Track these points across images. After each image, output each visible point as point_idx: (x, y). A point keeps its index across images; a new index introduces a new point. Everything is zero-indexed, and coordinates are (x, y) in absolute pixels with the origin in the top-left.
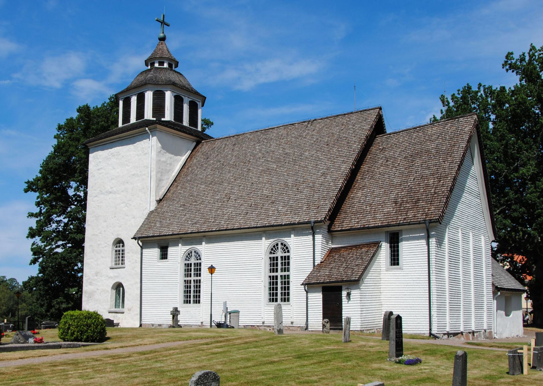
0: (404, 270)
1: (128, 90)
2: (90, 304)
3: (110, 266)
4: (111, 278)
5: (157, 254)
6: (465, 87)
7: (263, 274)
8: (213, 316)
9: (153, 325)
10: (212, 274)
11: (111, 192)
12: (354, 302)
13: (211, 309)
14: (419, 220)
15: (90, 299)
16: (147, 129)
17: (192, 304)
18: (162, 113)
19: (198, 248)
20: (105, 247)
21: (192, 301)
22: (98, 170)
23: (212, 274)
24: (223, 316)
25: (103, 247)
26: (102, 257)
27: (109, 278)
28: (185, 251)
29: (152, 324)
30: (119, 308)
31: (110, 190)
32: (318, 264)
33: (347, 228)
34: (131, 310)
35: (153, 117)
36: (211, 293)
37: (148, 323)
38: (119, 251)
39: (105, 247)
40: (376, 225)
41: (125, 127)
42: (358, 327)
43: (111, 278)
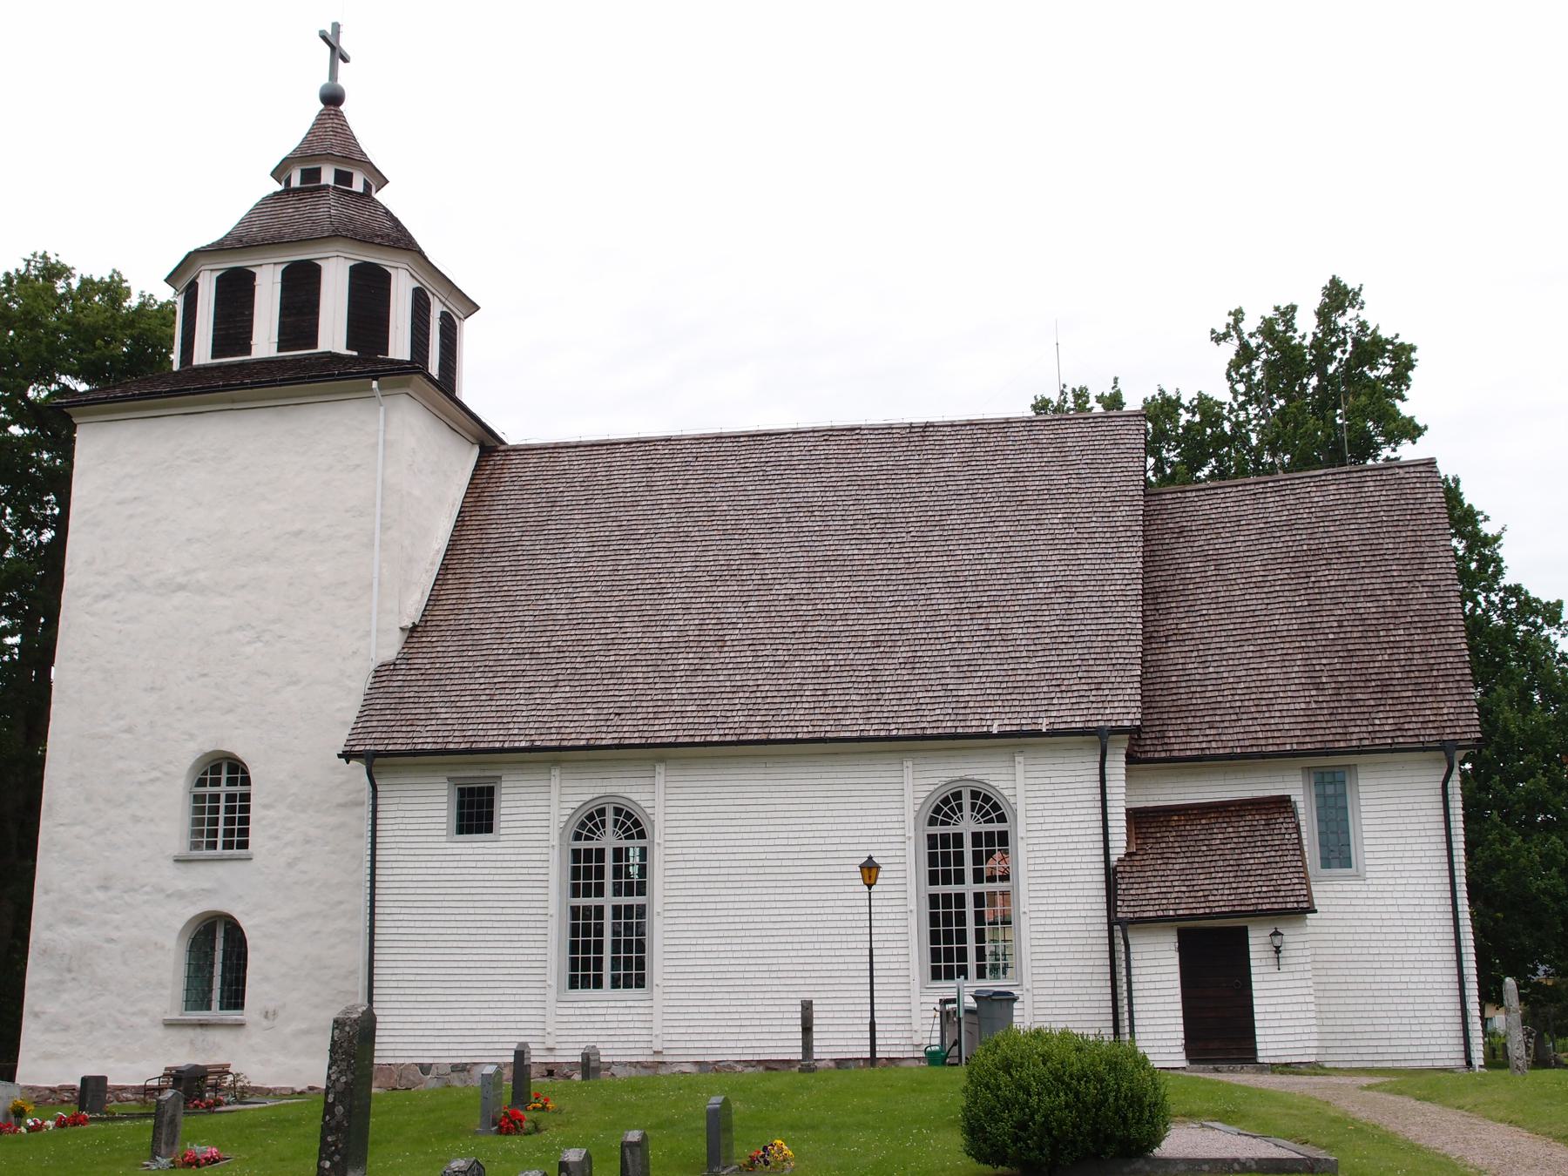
0: (1368, 882)
1: (234, 244)
2: (65, 996)
3: (176, 853)
4: (181, 895)
5: (503, 818)
6: (1408, 388)
7: (912, 889)
8: (878, 1028)
9: (425, 1069)
10: (870, 886)
11: (182, 587)
12: (1290, 976)
13: (872, 1004)
14: (1421, 739)
15: (68, 976)
16: (375, 384)
17: (607, 991)
18: (220, 329)
19: (634, 797)
20: (153, 781)
21: (607, 980)
22: (119, 503)
23: (870, 886)
24: (934, 1034)
25: (140, 784)
26: (136, 819)
27: (169, 896)
28: (576, 805)
29: (421, 1066)
30: (209, 1008)
31: (181, 580)
32: (1119, 860)
33: (463, 746)
34: (275, 1013)
35: (348, 348)
36: (871, 950)
37: (400, 1061)
38: (215, 798)
39: (153, 781)
40: (1282, 748)
41: (219, 367)
42: (1309, 1051)
43: (181, 895)
